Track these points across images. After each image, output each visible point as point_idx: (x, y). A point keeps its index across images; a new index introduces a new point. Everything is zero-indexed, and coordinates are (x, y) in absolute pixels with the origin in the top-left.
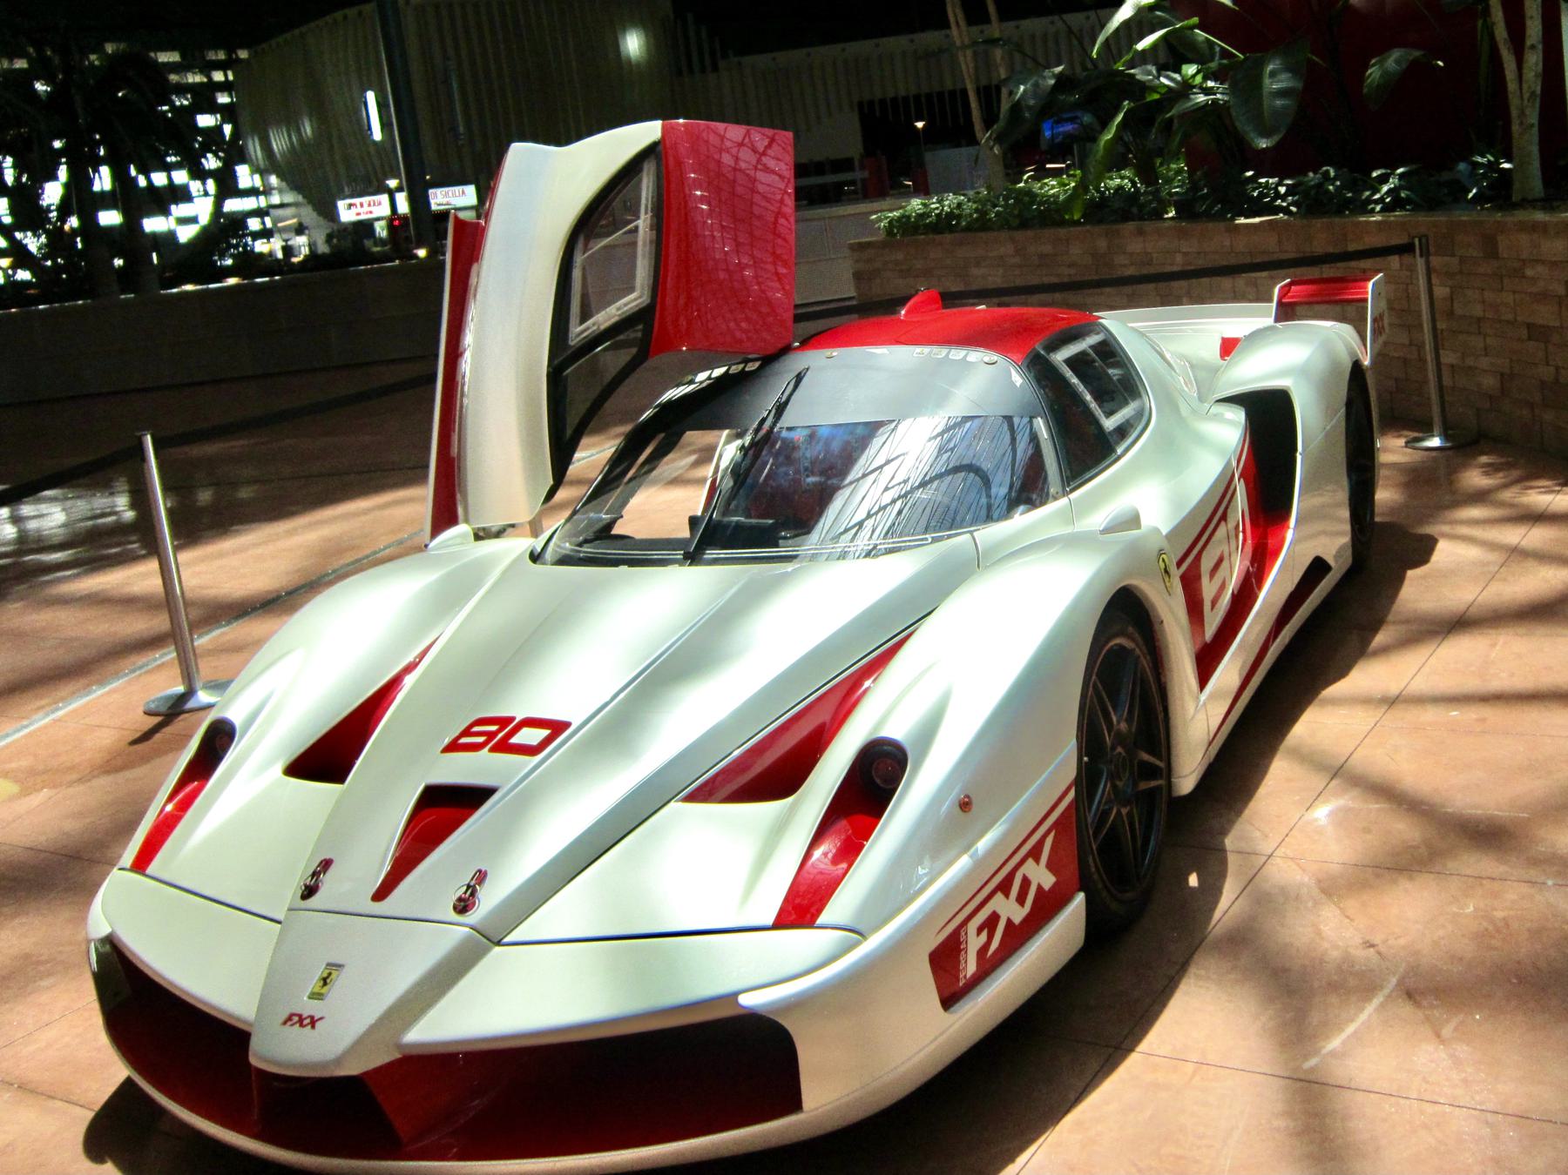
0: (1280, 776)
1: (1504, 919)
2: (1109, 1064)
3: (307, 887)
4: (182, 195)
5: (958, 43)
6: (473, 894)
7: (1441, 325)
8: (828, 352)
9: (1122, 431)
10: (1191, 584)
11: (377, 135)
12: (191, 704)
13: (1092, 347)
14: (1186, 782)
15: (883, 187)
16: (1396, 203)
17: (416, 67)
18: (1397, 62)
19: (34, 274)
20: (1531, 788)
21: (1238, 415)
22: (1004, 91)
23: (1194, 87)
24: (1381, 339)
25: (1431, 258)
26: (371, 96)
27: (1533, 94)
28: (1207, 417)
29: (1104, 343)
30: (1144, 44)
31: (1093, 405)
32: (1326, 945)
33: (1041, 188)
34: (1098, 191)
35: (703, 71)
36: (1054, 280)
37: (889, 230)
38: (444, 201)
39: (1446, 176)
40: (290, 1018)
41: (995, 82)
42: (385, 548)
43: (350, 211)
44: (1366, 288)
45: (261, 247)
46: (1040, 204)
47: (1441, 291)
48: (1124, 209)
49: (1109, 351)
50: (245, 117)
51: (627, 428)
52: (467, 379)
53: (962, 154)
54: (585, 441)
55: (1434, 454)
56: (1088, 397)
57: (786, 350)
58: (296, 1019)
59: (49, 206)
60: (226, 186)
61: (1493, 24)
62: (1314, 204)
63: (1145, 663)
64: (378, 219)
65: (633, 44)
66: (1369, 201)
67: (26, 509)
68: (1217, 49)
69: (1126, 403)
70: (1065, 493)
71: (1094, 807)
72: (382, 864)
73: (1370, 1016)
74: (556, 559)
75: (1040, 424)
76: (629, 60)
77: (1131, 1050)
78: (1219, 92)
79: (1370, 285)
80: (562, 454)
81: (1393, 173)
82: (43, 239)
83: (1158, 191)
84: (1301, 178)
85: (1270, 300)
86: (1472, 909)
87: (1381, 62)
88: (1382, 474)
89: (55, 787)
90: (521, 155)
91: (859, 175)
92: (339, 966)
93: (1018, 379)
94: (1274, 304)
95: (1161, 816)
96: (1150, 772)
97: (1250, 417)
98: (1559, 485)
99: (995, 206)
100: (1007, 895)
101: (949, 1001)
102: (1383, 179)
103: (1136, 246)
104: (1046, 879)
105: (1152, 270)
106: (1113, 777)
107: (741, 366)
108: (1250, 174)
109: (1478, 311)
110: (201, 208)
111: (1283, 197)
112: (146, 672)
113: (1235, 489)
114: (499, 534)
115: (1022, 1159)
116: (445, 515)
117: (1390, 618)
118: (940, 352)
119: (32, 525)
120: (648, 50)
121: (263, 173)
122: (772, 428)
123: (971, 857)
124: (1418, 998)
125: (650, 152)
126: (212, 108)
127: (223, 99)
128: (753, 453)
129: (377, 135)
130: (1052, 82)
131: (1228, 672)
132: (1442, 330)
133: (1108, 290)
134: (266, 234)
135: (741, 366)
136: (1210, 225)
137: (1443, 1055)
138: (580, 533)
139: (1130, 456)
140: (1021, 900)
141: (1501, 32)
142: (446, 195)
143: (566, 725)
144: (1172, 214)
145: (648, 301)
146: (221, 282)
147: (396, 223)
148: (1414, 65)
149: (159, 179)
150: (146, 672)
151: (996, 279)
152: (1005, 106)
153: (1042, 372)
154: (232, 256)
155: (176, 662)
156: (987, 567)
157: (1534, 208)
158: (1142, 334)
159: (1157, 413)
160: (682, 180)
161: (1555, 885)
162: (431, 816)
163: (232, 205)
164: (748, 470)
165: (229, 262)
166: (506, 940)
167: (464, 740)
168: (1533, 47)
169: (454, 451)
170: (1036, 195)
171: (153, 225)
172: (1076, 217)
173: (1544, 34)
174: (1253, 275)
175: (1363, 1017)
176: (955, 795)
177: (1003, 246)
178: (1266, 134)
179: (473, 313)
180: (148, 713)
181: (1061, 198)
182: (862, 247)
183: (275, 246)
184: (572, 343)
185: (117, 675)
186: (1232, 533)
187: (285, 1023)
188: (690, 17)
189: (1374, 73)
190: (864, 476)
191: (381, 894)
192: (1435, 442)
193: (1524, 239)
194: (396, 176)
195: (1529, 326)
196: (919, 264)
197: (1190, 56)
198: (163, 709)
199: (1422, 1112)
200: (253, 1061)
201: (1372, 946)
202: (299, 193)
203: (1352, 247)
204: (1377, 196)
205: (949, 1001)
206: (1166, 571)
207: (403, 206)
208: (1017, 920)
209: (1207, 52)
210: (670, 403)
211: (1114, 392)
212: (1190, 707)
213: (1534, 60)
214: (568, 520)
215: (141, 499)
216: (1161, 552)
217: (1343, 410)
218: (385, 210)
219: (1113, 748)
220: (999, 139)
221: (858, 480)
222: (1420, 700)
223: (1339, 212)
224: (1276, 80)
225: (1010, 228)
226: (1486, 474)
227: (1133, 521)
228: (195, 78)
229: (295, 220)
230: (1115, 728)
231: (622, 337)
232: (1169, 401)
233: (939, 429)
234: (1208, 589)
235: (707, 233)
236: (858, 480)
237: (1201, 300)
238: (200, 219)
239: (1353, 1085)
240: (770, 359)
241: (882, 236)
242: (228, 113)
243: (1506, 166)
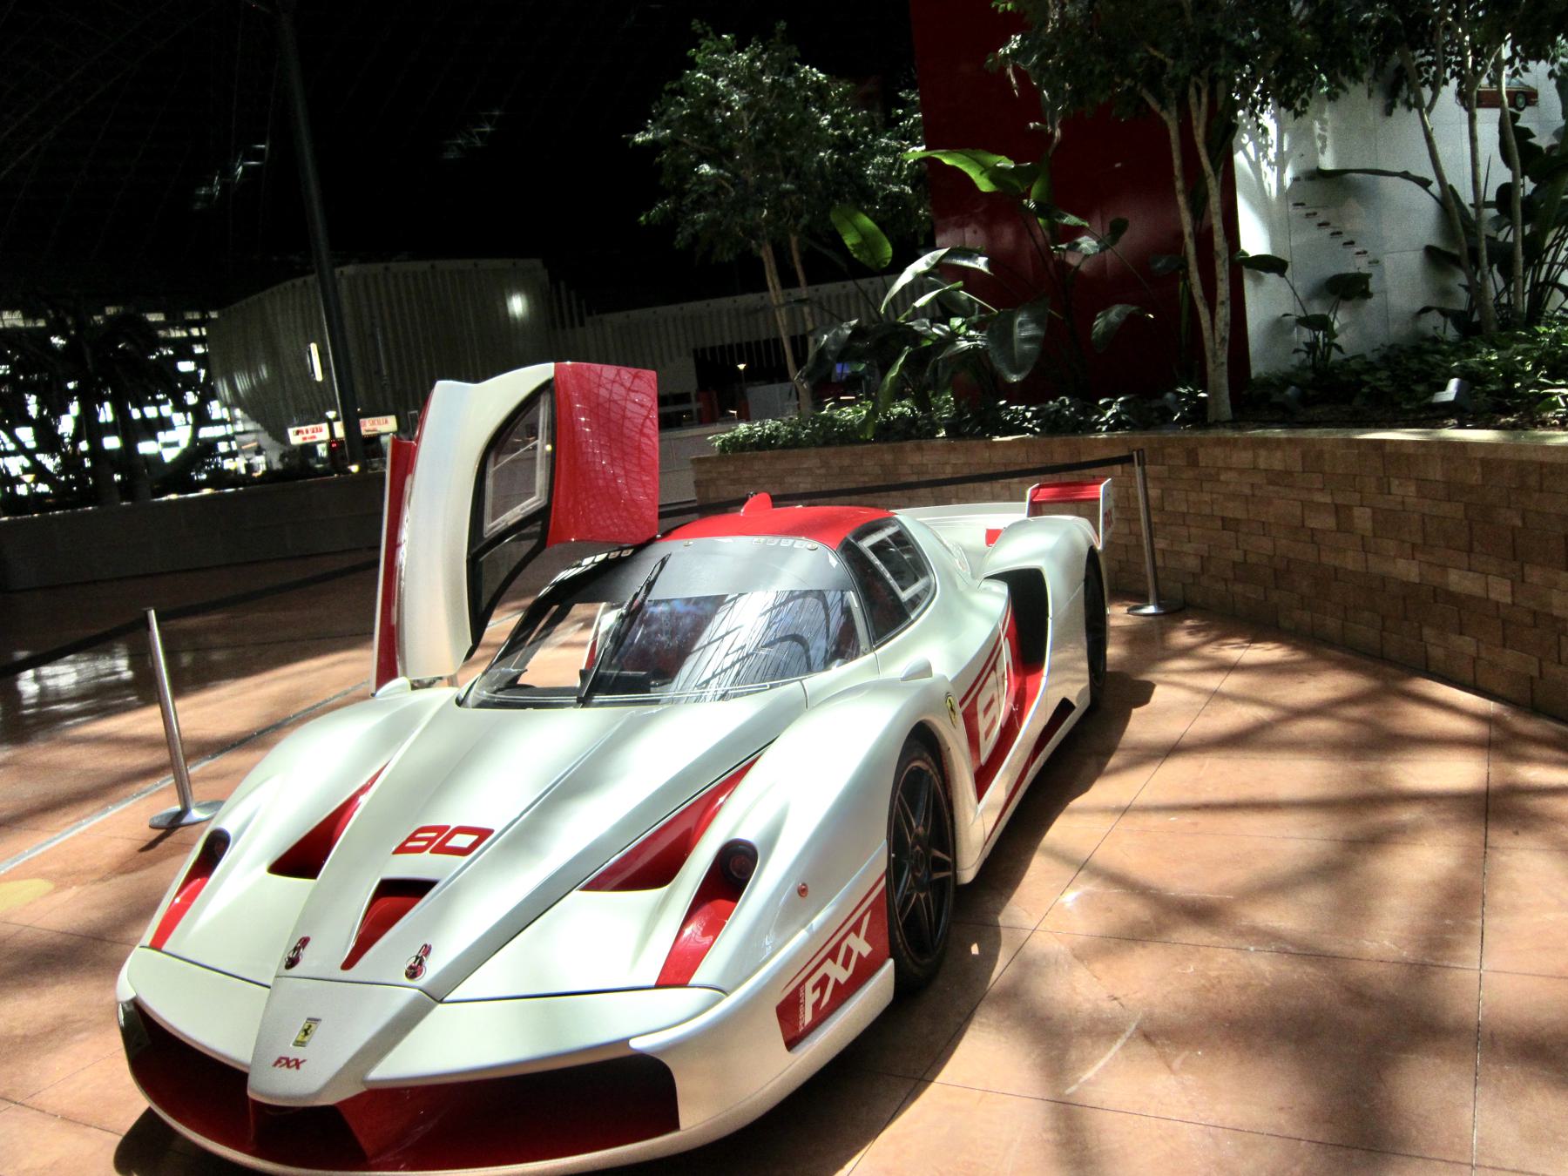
0: (1039, 872)
1: (1217, 977)
2: (914, 1094)
3: (289, 959)
4: (165, 424)
5: (775, 302)
6: (420, 964)
7: (1155, 519)
8: (685, 542)
9: (914, 602)
10: (970, 718)
11: (319, 377)
12: (186, 820)
13: (889, 537)
14: (968, 873)
15: (715, 415)
16: (1118, 424)
17: (349, 322)
18: (1118, 315)
19: (51, 488)
20: (1238, 876)
21: (1002, 589)
22: (811, 340)
23: (960, 335)
24: (1110, 530)
25: (1146, 467)
26: (314, 347)
27: (1223, 339)
28: (978, 590)
30: (920, 302)
31: (892, 582)
32: (1080, 998)
33: (840, 415)
34: (884, 416)
35: (563, 327)
36: (853, 485)
37: (723, 448)
38: (371, 428)
39: (1156, 403)
40: (279, 1061)
41: (800, 332)
42: (334, 697)
43: (296, 437)
44: (1098, 489)
45: (228, 464)
46: (841, 427)
47: (1154, 493)
48: (891, 432)
49: (902, 539)
50: (215, 361)
51: (529, 601)
52: (403, 567)
53: (776, 389)
54: (496, 612)
55: (1150, 618)
56: (888, 575)
57: (652, 541)
58: (284, 1061)
59: (63, 434)
61: (1191, 285)
62: (1053, 425)
63: (937, 781)
64: (320, 442)
65: (517, 305)
66: (1097, 423)
67: (46, 670)
68: (977, 306)
69: (916, 580)
70: (872, 650)
71: (900, 891)
72: (348, 943)
73: (1115, 1054)
74: (476, 703)
75: (852, 598)
76: (515, 318)
77: (931, 1081)
78: (979, 339)
79: (1101, 487)
80: (479, 622)
81: (1115, 401)
82: (58, 460)
83: (930, 417)
84: (1043, 406)
85: (1023, 500)
86: (1192, 970)
87: (1105, 315)
88: (1111, 635)
89: (84, 884)
90: (445, 392)
91: (695, 406)
92: (316, 1020)
93: (834, 561)
94: (1027, 503)
95: (949, 902)
96: (940, 865)
98: (1246, 642)
99: (804, 429)
100: (835, 961)
101: (791, 1044)
102: (1108, 406)
103: (915, 459)
106: (914, 869)
107: (618, 553)
108: (1002, 402)
109: (1184, 508)
111: (1029, 421)
112: (151, 795)
113: (1001, 648)
114: (430, 685)
115: (849, 1166)
116: (388, 669)
117: (1120, 746)
118: (772, 541)
119: (50, 683)
120: (530, 313)
121: (230, 407)
122: (643, 600)
123: (808, 931)
124: (1153, 1038)
125: (546, 387)
126: (190, 356)
127: (199, 350)
128: (634, 615)
129: (319, 377)
130: (849, 332)
131: (998, 789)
132: (1156, 523)
133: (894, 493)
134: (232, 455)
135: (618, 553)
136: (974, 442)
137: (1174, 1083)
138: (495, 684)
139: (921, 621)
141: (1198, 291)
142: (373, 423)
143: (490, 832)
144: (943, 433)
145: (546, 503)
146: (197, 492)
147: (334, 445)
148: (1131, 318)
149: (151, 412)
150: (151, 795)
151: (805, 485)
152: (812, 352)
153: (851, 554)
154: (206, 472)
155: (175, 787)
156: (814, 707)
157: (1225, 427)
158: (927, 527)
160: (571, 408)
161: (1256, 950)
162: (387, 903)
163: (206, 432)
164: (626, 634)
165: (204, 477)
166: (447, 999)
167: (410, 844)
168: (1223, 303)
169: (394, 621)
170: (837, 420)
171: (146, 448)
172: (868, 437)
173: (1231, 294)
174: (1007, 481)
175: (1111, 1054)
176: (792, 886)
177: (811, 460)
178: (1016, 372)
179: (408, 515)
180: (153, 827)
181: (857, 423)
182: (699, 461)
183: (238, 465)
184: (486, 536)
185: (127, 797)
186: (1000, 680)
187: (275, 1065)
188: (562, 285)
189: (1099, 324)
190: (709, 644)
191: (349, 964)
192: (1151, 609)
193: (1218, 451)
194: (333, 407)
195: (1223, 519)
196: (747, 474)
197: (956, 311)
198: (164, 824)
199: (1159, 1127)
200: (250, 1094)
201: (1115, 999)
202: (258, 422)
203: (1084, 459)
204: (1103, 419)
205: (791, 1044)
206: (952, 709)
207: (340, 432)
208: (842, 980)
209: (969, 309)
210: (563, 582)
211: (903, 572)
212: (971, 816)
213: (1223, 312)
214: (485, 673)
215: (141, 658)
216: (948, 695)
218: (324, 435)
219: (913, 847)
220: (808, 377)
221: (705, 647)
222: (1146, 809)
223: (1074, 431)
224: (1024, 329)
225: (817, 446)
226: (1191, 634)
227: (926, 670)
228: (177, 334)
229: (255, 444)
230: (915, 831)
231: (524, 531)
232: (949, 578)
233: (770, 606)
234: (983, 724)
235: (590, 450)
236: (705, 647)
237: (966, 500)
238: (180, 443)
239: (1105, 1106)
240: (640, 548)
241: (716, 453)
242: (201, 361)
243: (1203, 395)
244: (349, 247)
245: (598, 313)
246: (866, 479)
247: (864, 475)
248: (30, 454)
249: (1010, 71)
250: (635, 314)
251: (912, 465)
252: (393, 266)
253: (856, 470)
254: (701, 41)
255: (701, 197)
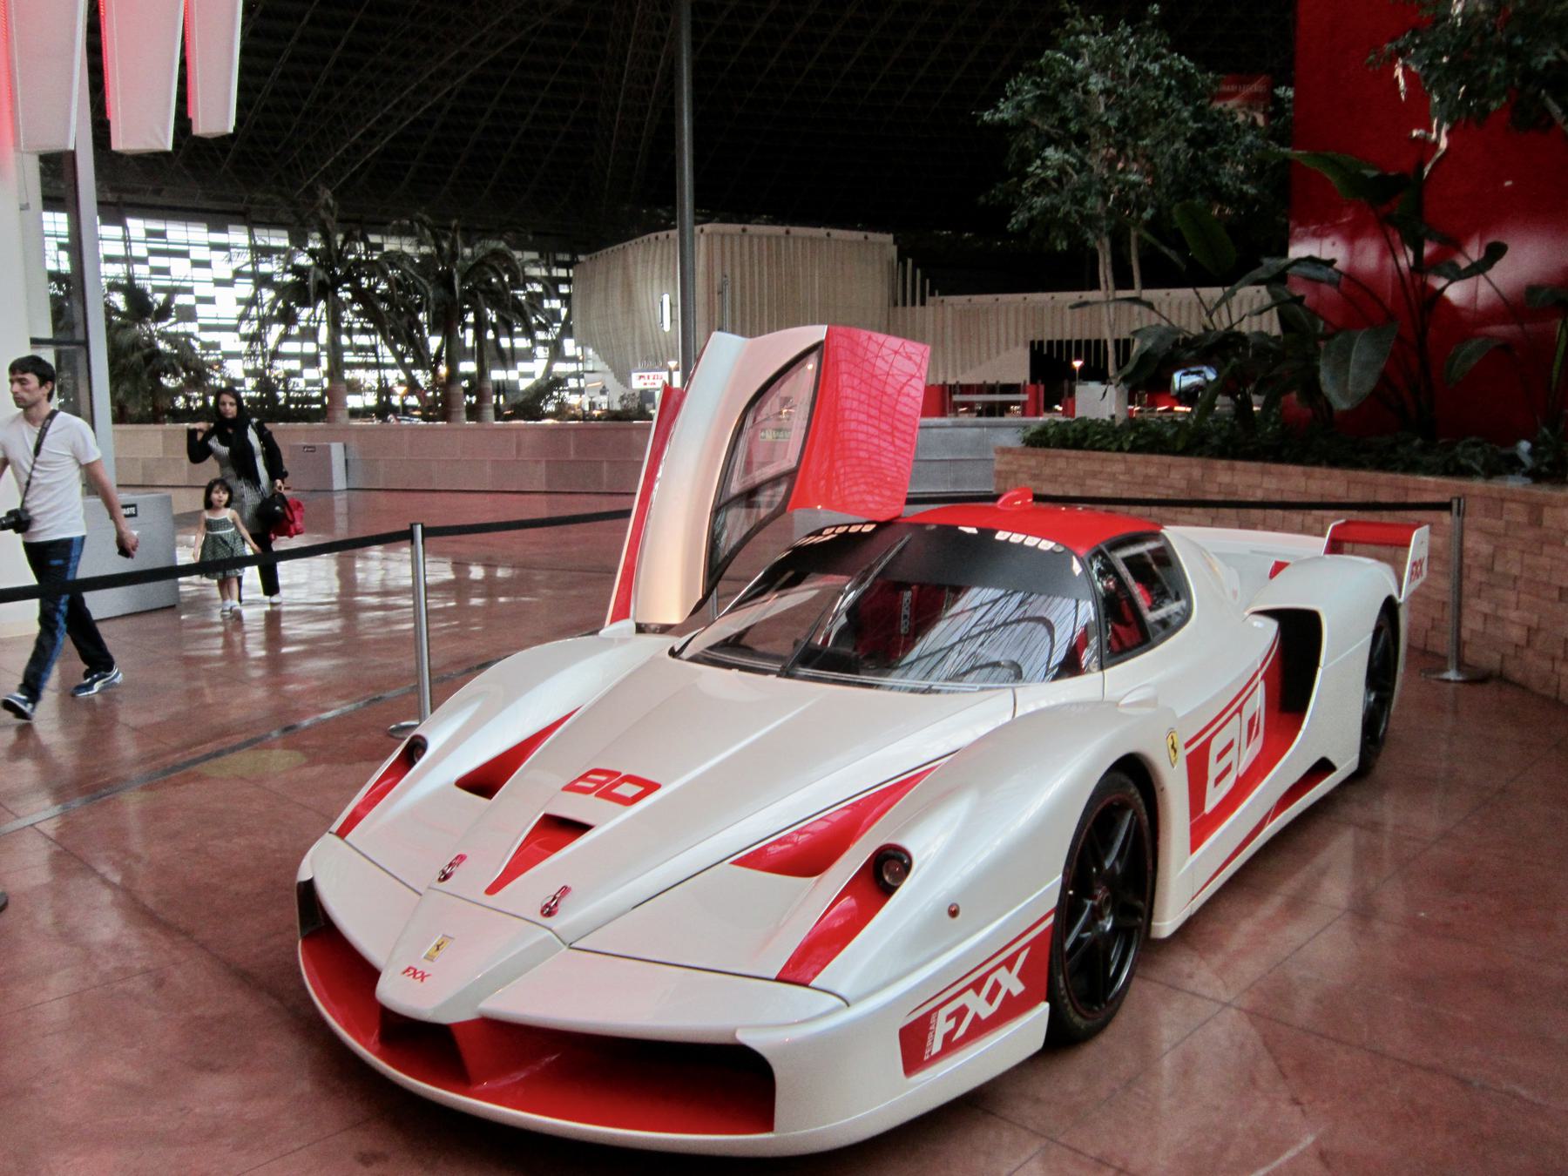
4: (529, 355)
13: (1149, 551)
21: (1272, 626)
24: (1418, 582)
29: (1161, 549)
35: (914, 303)
40: (408, 970)
45: (573, 400)
49: (1165, 558)
50: (576, 302)
58: (412, 971)
60: (556, 352)
85: (1322, 535)
97: (1283, 630)
104: (1017, 988)
105: (1235, 498)
109: (1515, 571)
110: (538, 367)
127: (564, 289)
134: (580, 391)
140: (990, 999)
159: (1198, 612)
163: (560, 368)
167: (581, 784)
171: (497, 375)
188: (910, 261)
191: (493, 889)
194: (675, 357)
202: (607, 363)
217: (1370, 636)
229: (599, 383)
234: (1214, 770)
242: (566, 299)
244: (713, 206)
245: (940, 294)
246: (1171, 492)
247: (1170, 487)
248: (407, 368)
249: (1399, 72)
250: (976, 298)
251: (1220, 484)
252: (751, 228)
253: (1160, 481)
254: (1067, 20)
255: (1044, 181)
